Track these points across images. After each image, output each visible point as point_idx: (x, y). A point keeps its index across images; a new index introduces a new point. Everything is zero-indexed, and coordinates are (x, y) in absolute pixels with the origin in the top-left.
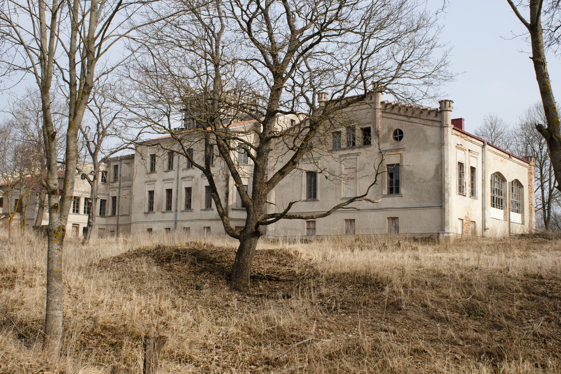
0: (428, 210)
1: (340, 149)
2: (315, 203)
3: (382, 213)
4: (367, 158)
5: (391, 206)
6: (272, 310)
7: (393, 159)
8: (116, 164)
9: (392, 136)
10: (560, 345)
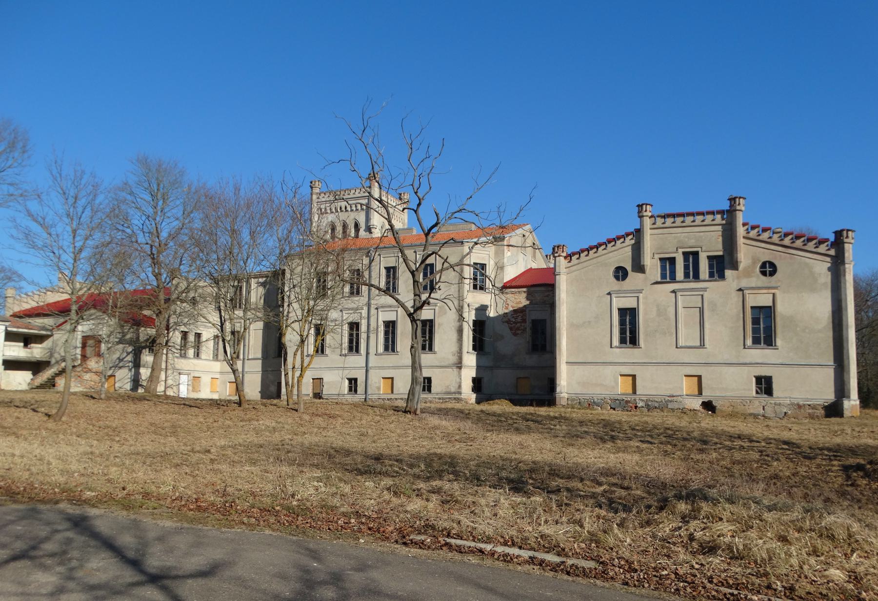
0: (818, 369)
1: (673, 279)
2: (636, 351)
3: (746, 369)
4: (724, 298)
5: (760, 361)
6: (679, 506)
7: (764, 300)
8: (391, 317)
9: (758, 269)
10: (2, 419)
